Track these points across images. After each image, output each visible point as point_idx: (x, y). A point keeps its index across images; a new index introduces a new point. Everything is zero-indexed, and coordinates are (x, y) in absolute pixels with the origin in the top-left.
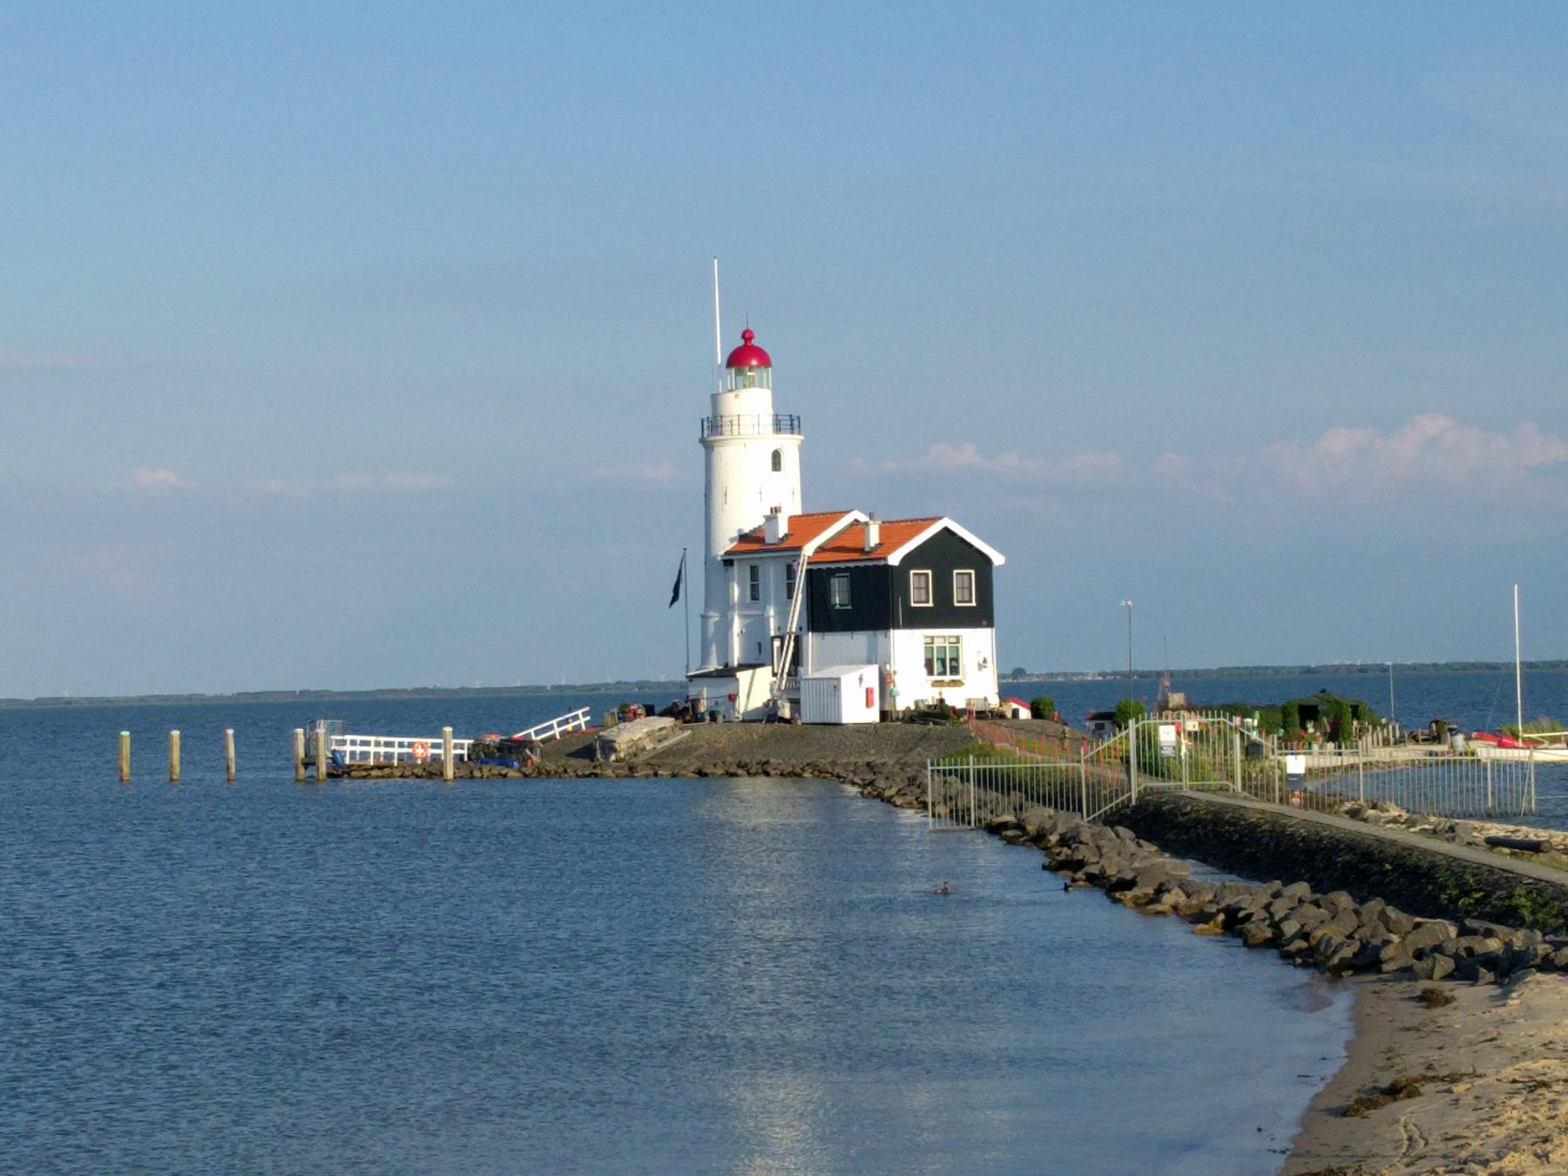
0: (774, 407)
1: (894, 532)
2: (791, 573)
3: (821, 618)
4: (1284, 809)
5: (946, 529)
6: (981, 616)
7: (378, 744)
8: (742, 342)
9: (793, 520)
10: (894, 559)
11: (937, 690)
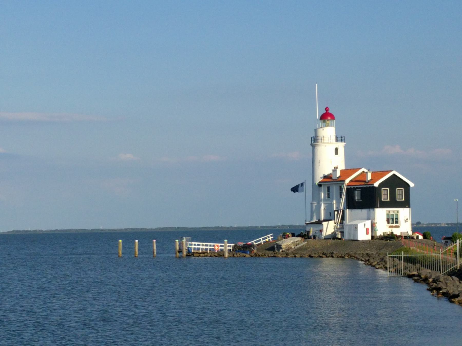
2: (341, 189)
3: (352, 204)
6: (406, 204)
8: (325, 112)
10: (376, 184)
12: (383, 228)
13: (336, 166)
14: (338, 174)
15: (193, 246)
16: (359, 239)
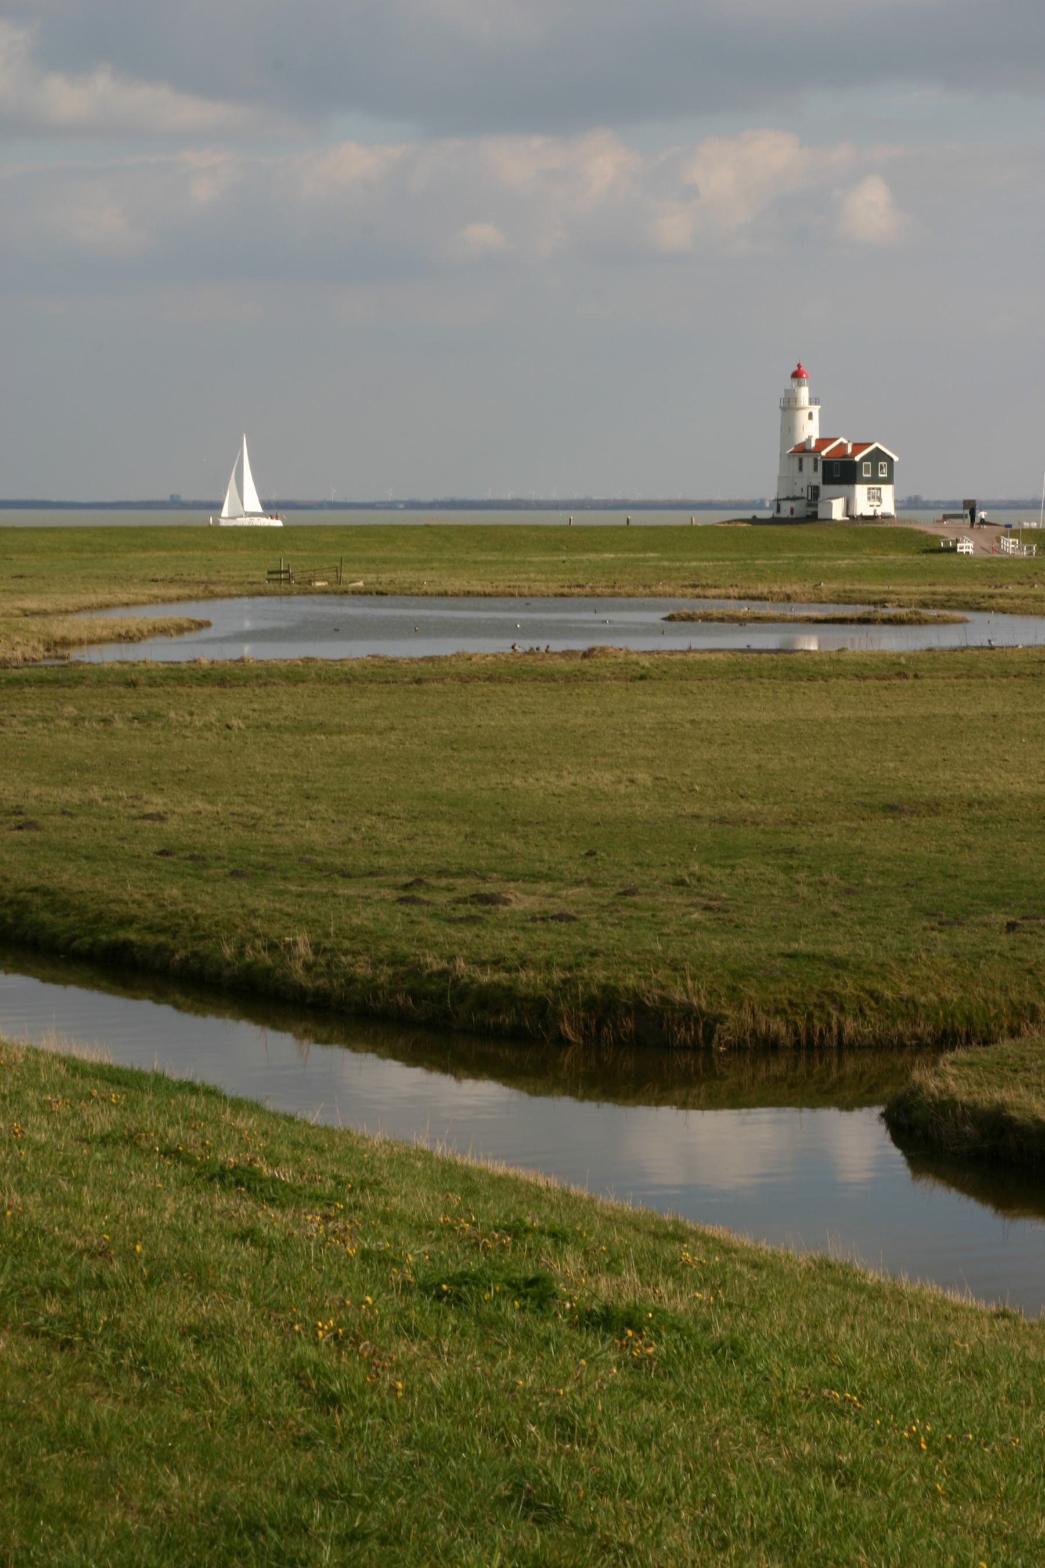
1: (858, 447)
2: (816, 461)
3: (828, 479)
5: (877, 449)
9: (817, 441)
10: (857, 458)
11: (872, 509)
12: (863, 506)
13: (212, 621)
14: (813, 444)
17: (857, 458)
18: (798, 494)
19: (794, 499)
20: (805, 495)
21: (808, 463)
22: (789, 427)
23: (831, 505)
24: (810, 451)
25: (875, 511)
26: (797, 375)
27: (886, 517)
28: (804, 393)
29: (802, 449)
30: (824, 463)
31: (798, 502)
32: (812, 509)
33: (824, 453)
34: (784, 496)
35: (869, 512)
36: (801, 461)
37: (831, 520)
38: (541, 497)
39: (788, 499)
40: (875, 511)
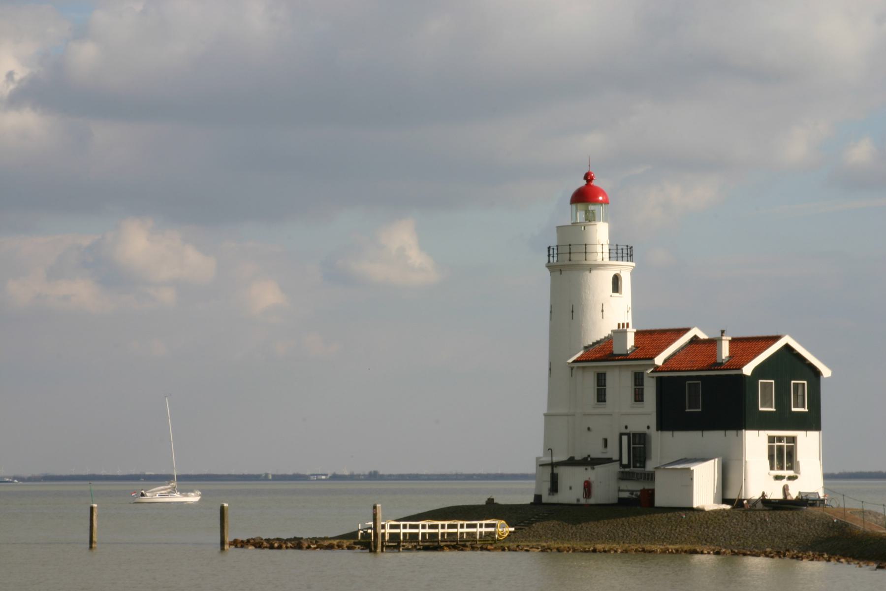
0: (610, 238)
2: (639, 379)
3: (671, 417)
4: (462, 522)
5: (787, 347)
6: (811, 422)
7: (424, 527)
8: (584, 183)
10: (748, 370)
12: (760, 481)
14: (630, 342)
15: (388, 530)
16: (695, 506)
17: (748, 370)
18: (597, 452)
19: (590, 462)
20: (612, 452)
21: (620, 383)
22: (567, 307)
23: (690, 473)
24: (625, 357)
25: (785, 489)
26: (584, 196)
27: (804, 502)
28: (600, 234)
29: (604, 353)
30: (660, 382)
31: (600, 469)
32: (637, 486)
33: (659, 360)
34: (564, 458)
35: (775, 494)
36: (601, 379)
37: (692, 509)
38: (110, 473)
39: (571, 462)
40: (785, 489)
